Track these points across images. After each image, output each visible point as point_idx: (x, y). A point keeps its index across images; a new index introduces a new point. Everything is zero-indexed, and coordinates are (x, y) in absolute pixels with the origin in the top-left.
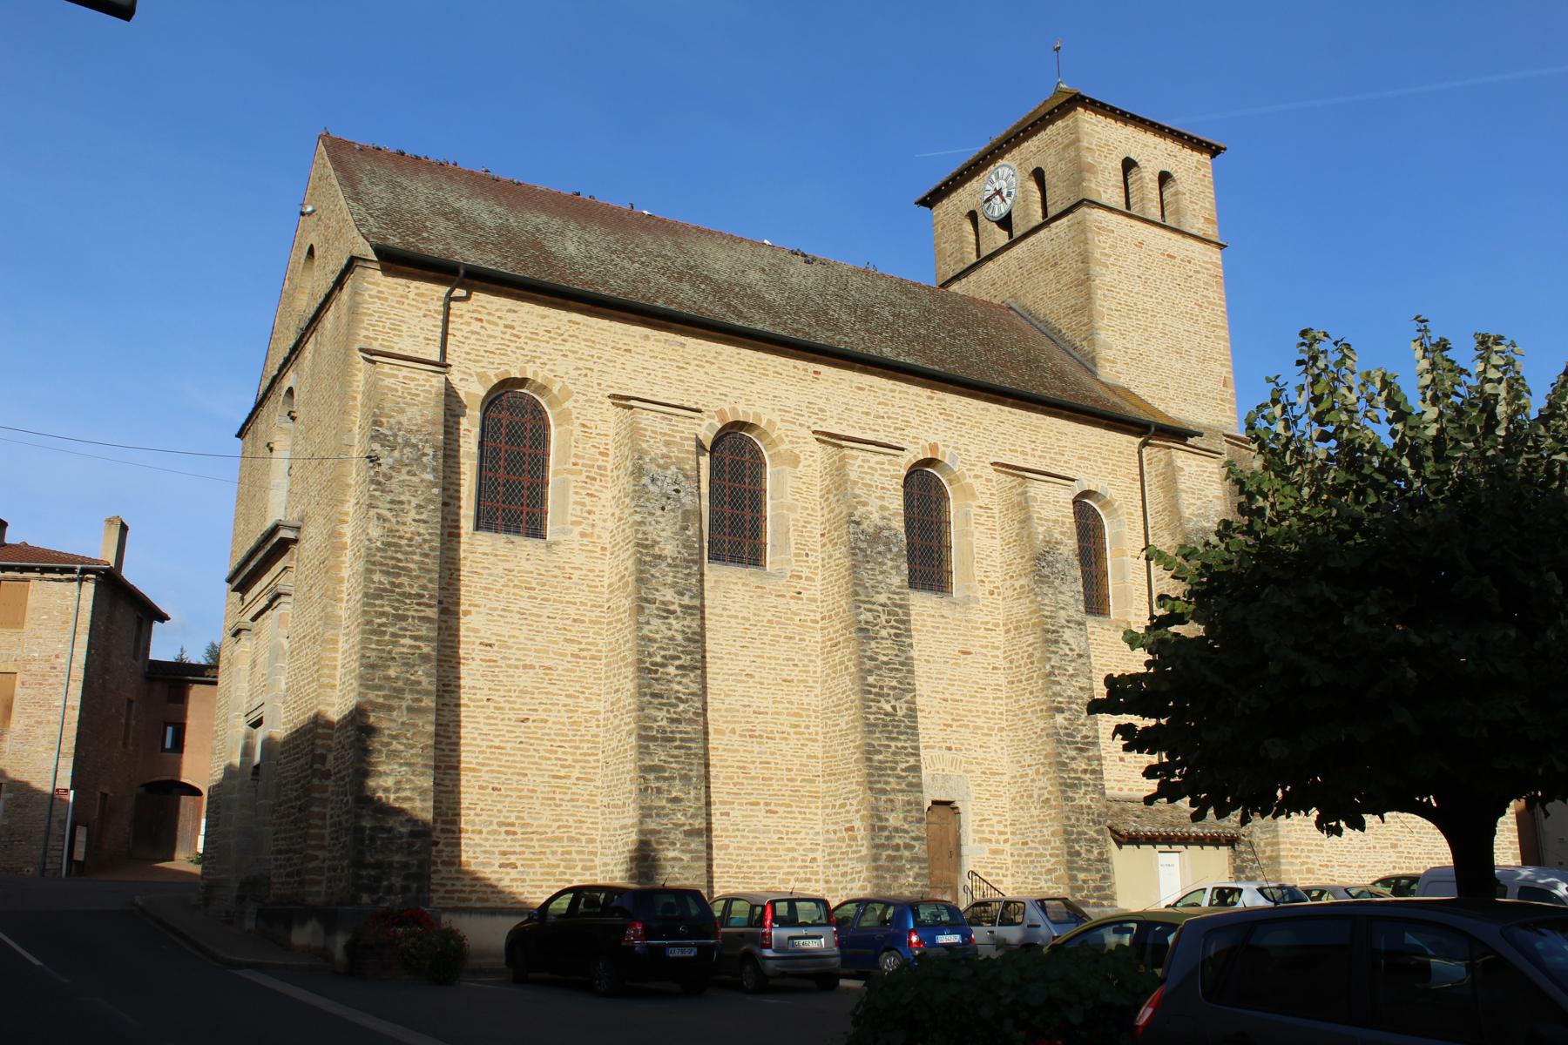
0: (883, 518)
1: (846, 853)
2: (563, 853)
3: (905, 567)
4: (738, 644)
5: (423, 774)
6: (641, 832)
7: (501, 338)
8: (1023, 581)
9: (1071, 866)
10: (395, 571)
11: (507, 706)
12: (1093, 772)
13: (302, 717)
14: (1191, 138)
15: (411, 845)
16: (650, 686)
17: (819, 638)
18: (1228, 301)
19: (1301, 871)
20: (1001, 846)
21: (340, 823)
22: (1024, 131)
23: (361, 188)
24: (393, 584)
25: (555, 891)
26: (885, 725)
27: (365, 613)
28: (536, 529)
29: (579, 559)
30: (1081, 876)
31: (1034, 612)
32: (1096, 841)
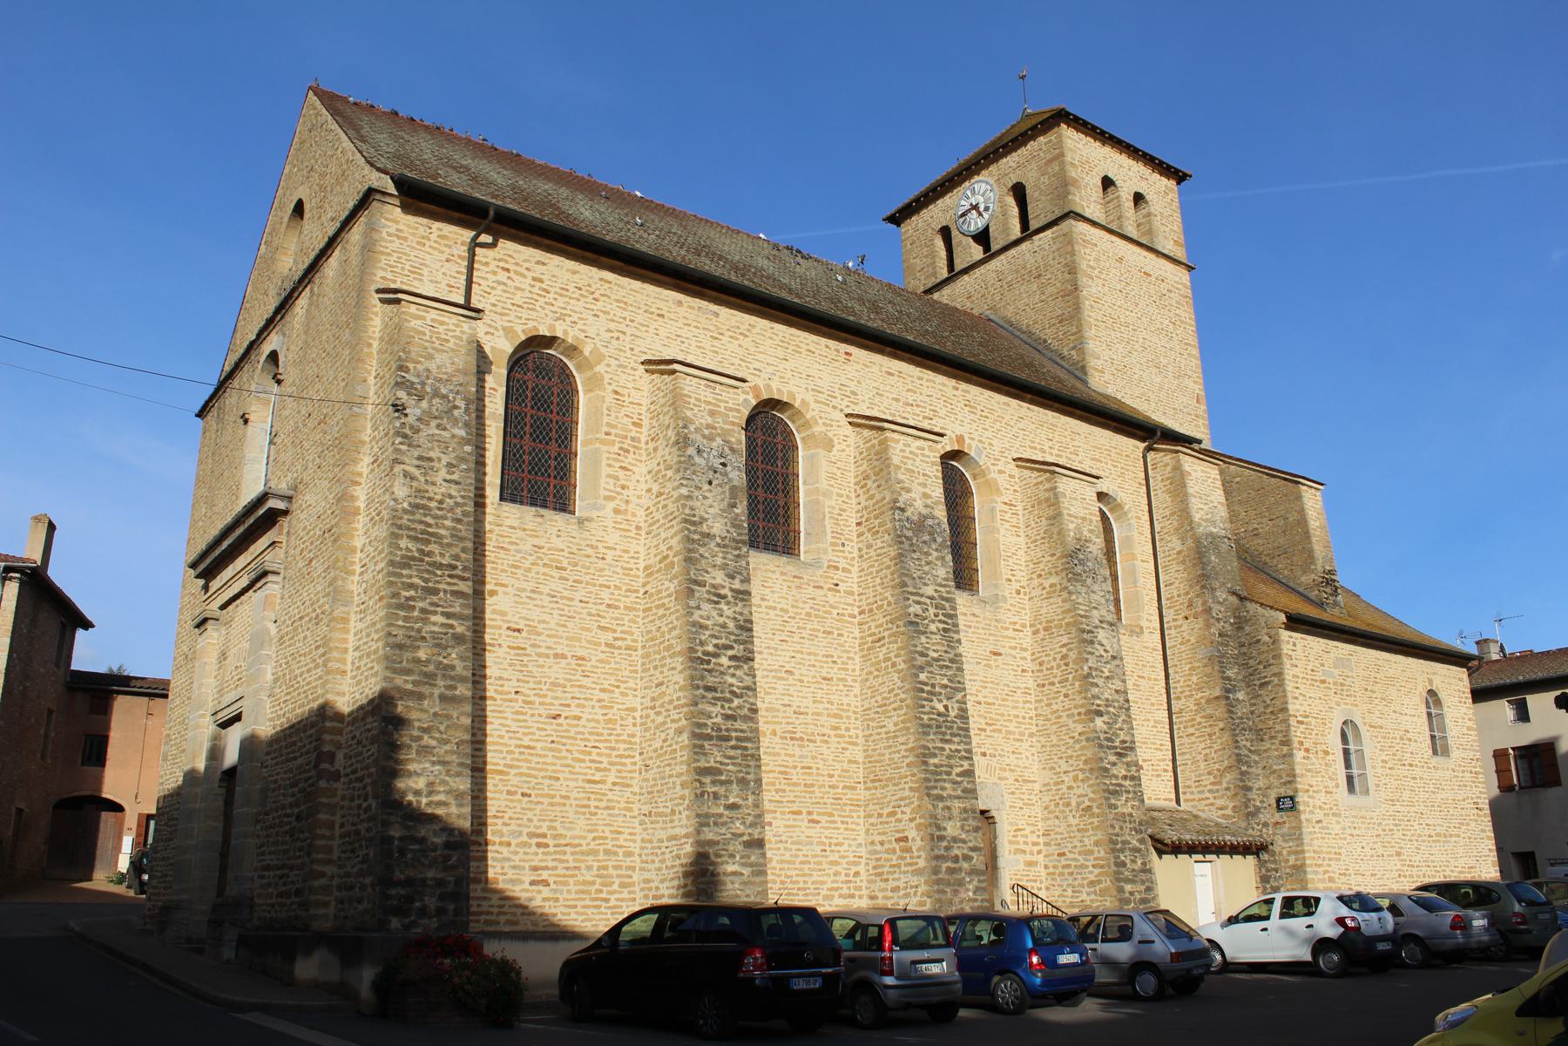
0: (926, 506)
1: (898, 866)
2: (599, 868)
3: (949, 558)
4: (777, 638)
5: (458, 774)
6: (699, 843)
7: (532, 291)
9: (1118, 878)
11: (537, 700)
12: (1133, 778)
13: (297, 708)
14: (1161, 163)
15: (446, 858)
16: (702, 678)
17: (857, 634)
18: (1198, 320)
19: (1323, 880)
20: (1035, 858)
21: (357, 833)
24: (421, 551)
25: (637, 909)
26: (939, 727)
27: (391, 583)
28: (561, 501)
29: (613, 538)
30: (1128, 887)
31: (1069, 611)
32: (1139, 850)
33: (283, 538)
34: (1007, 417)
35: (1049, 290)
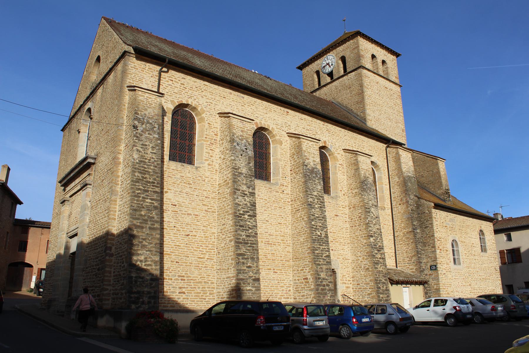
0: (314, 165)
2: (202, 288)
3: (322, 182)
4: (263, 209)
5: (155, 255)
6: (238, 279)
7: (181, 88)
8: (356, 191)
9: (378, 293)
10: (144, 172)
11: (181, 229)
12: (383, 258)
14: (391, 50)
15: (151, 284)
16: (239, 222)
17: (290, 208)
20: (349, 285)
24: (143, 177)
26: (318, 240)
27: (132, 188)
29: (208, 174)
30: (381, 296)
31: (362, 201)
33: (93, 173)
34: (341, 135)
35: (353, 93)
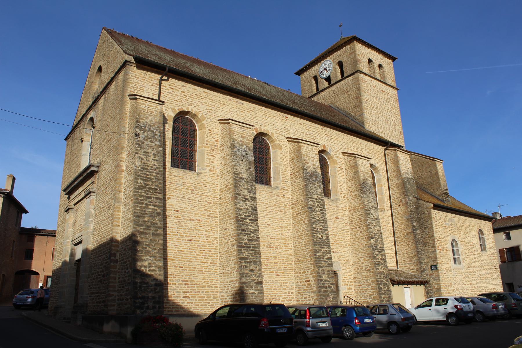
1: (307, 290)
2: (206, 292)
3: (322, 186)
4: (265, 213)
5: (159, 260)
6: (241, 283)
7: (181, 96)
8: (356, 193)
9: (379, 293)
10: (146, 179)
11: (184, 235)
12: (384, 259)
13: (104, 239)
14: (388, 54)
15: (155, 289)
16: (241, 227)
19: (447, 293)
20: (351, 287)
21: (124, 281)
22: (335, 49)
23: (122, 42)
24: (145, 184)
26: (319, 243)
27: (135, 195)
29: (209, 179)
30: (383, 296)
31: (361, 203)
33: (96, 180)
34: (339, 139)
35: (351, 97)
